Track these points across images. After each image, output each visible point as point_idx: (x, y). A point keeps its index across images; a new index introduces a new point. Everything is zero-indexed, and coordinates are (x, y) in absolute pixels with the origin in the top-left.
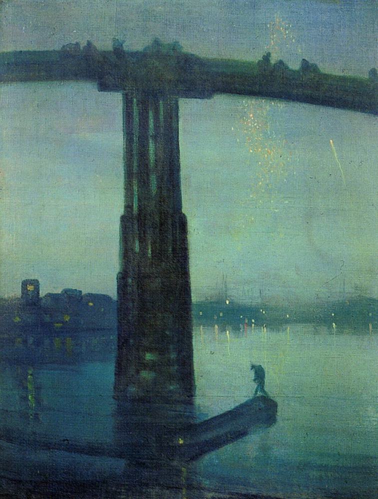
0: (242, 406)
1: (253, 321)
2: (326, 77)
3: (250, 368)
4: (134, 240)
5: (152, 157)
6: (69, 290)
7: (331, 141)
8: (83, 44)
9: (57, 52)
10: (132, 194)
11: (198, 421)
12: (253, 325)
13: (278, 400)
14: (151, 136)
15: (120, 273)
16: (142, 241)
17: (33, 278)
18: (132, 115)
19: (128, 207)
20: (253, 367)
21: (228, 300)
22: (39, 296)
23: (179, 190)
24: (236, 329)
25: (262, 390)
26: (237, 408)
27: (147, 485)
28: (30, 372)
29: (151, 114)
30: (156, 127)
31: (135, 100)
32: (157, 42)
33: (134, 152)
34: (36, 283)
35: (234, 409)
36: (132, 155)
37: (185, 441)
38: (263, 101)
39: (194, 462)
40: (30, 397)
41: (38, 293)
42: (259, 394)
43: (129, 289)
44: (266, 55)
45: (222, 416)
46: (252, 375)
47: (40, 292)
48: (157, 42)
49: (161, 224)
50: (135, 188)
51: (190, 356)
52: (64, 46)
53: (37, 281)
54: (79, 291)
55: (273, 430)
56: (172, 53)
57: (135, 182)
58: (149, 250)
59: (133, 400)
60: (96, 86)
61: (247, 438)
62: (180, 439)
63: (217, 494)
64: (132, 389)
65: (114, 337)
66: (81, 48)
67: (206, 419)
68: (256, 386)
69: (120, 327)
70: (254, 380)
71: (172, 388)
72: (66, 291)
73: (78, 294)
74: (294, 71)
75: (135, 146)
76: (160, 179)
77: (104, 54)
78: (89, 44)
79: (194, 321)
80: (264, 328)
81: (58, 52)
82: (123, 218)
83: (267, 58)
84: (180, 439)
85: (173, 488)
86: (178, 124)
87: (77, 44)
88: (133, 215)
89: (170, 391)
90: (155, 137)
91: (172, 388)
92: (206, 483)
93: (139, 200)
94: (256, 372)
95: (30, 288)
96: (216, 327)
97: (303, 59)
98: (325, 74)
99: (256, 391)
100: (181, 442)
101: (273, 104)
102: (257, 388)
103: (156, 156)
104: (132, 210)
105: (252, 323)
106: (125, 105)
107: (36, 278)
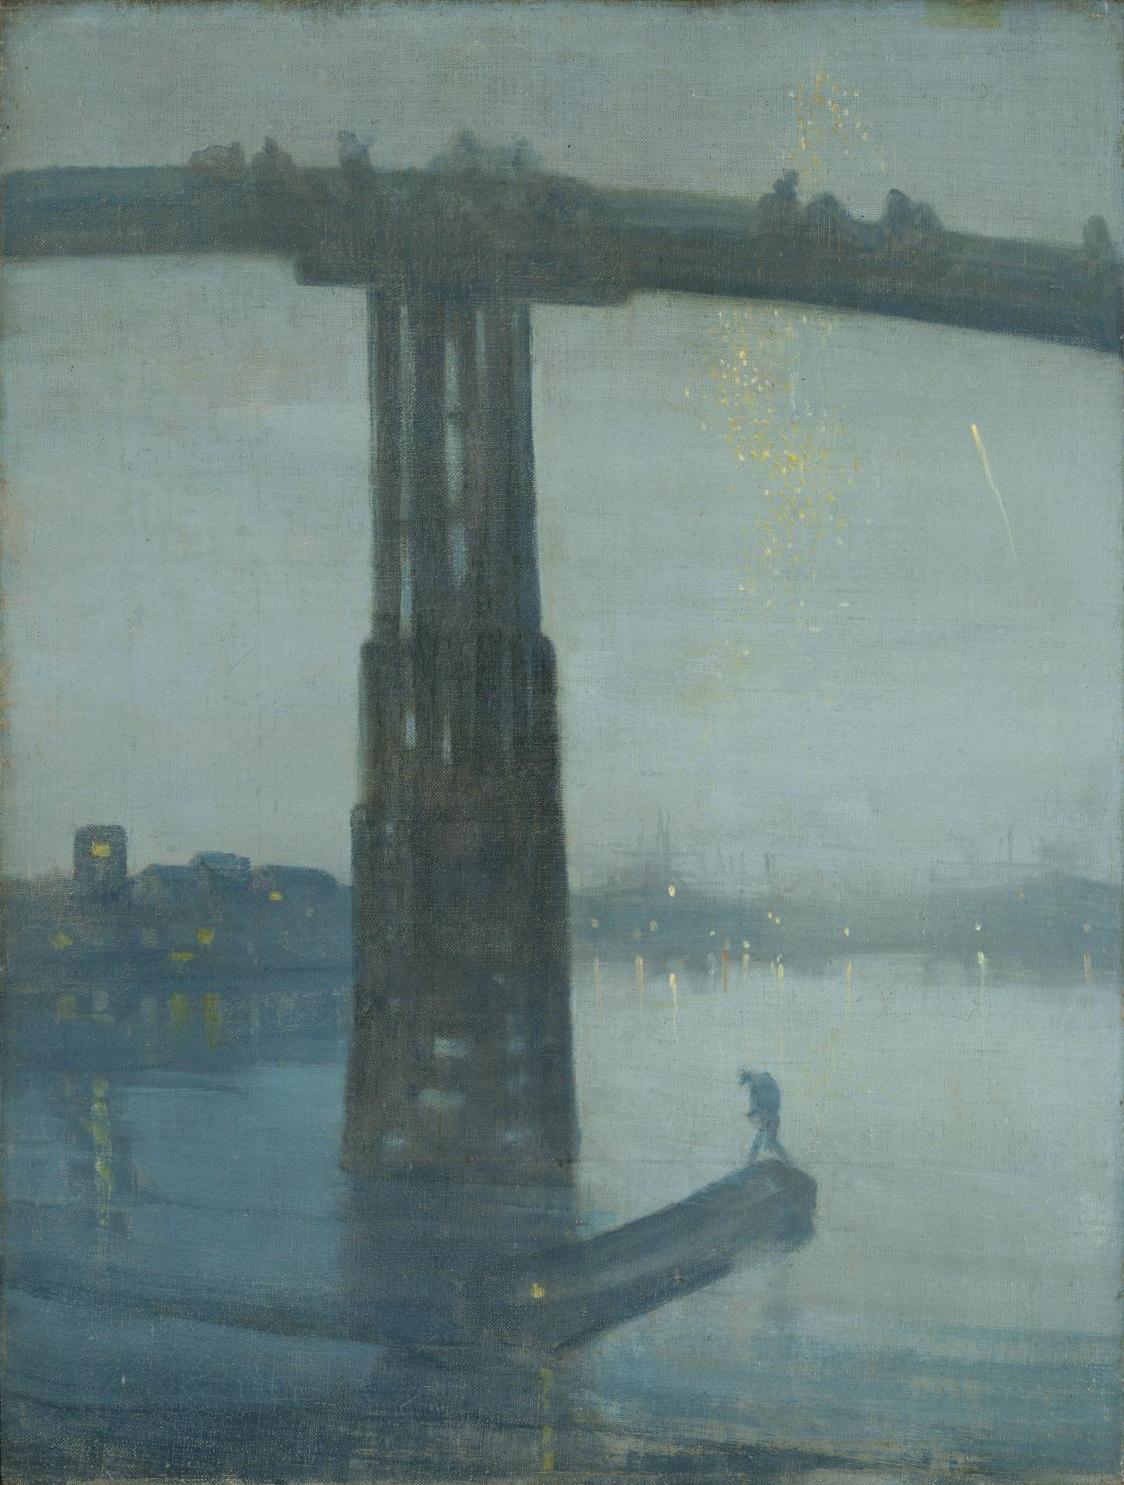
0: (715, 1190)
1: (747, 945)
2: (961, 240)
5: (454, 477)
6: (214, 857)
8: (252, 150)
9: (176, 169)
10: (398, 580)
11: (585, 1234)
12: (747, 957)
14: (452, 415)
15: (358, 808)
18: (397, 356)
19: (386, 618)
21: (673, 884)
22: (125, 873)
25: (773, 1142)
26: (697, 1198)
28: (99, 1092)
30: (468, 389)
31: (404, 311)
32: (467, 142)
34: (115, 837)
36: (396, 469)
38: (776, 312)
40: (98, 1163)
41: (124, 865)
42: (765, 1154)
46: (743, 1100)
47: (129, 862)
48: (467, 142)
49: (482, 670)
50: (406, 565)
52: (196, 154)
55: (805, 1257)
57: (405, 546)
60: (290, 271)
65: (344, 992)
66: (248, 160)
70: (750, 1115)
71: (510, 1137)
72: (204, 861)
74: (866, 227)
75: (405, 439)
76: (479, 541)
78: (271, 148)
79: (576, 946)
82: (372, 653)
83: (785, 189)
84: (535, 1285)
90: (463, 420)
91: (510, 1137)
95: (101, 850)
96: (640, 961)
97: (893, 191)
98: (955, 235)
99: (756, 1147)
100: (538, 1293)
102: (759, 1138)
103: (465, 472)
104: (397, 628)
107: (119, 822)
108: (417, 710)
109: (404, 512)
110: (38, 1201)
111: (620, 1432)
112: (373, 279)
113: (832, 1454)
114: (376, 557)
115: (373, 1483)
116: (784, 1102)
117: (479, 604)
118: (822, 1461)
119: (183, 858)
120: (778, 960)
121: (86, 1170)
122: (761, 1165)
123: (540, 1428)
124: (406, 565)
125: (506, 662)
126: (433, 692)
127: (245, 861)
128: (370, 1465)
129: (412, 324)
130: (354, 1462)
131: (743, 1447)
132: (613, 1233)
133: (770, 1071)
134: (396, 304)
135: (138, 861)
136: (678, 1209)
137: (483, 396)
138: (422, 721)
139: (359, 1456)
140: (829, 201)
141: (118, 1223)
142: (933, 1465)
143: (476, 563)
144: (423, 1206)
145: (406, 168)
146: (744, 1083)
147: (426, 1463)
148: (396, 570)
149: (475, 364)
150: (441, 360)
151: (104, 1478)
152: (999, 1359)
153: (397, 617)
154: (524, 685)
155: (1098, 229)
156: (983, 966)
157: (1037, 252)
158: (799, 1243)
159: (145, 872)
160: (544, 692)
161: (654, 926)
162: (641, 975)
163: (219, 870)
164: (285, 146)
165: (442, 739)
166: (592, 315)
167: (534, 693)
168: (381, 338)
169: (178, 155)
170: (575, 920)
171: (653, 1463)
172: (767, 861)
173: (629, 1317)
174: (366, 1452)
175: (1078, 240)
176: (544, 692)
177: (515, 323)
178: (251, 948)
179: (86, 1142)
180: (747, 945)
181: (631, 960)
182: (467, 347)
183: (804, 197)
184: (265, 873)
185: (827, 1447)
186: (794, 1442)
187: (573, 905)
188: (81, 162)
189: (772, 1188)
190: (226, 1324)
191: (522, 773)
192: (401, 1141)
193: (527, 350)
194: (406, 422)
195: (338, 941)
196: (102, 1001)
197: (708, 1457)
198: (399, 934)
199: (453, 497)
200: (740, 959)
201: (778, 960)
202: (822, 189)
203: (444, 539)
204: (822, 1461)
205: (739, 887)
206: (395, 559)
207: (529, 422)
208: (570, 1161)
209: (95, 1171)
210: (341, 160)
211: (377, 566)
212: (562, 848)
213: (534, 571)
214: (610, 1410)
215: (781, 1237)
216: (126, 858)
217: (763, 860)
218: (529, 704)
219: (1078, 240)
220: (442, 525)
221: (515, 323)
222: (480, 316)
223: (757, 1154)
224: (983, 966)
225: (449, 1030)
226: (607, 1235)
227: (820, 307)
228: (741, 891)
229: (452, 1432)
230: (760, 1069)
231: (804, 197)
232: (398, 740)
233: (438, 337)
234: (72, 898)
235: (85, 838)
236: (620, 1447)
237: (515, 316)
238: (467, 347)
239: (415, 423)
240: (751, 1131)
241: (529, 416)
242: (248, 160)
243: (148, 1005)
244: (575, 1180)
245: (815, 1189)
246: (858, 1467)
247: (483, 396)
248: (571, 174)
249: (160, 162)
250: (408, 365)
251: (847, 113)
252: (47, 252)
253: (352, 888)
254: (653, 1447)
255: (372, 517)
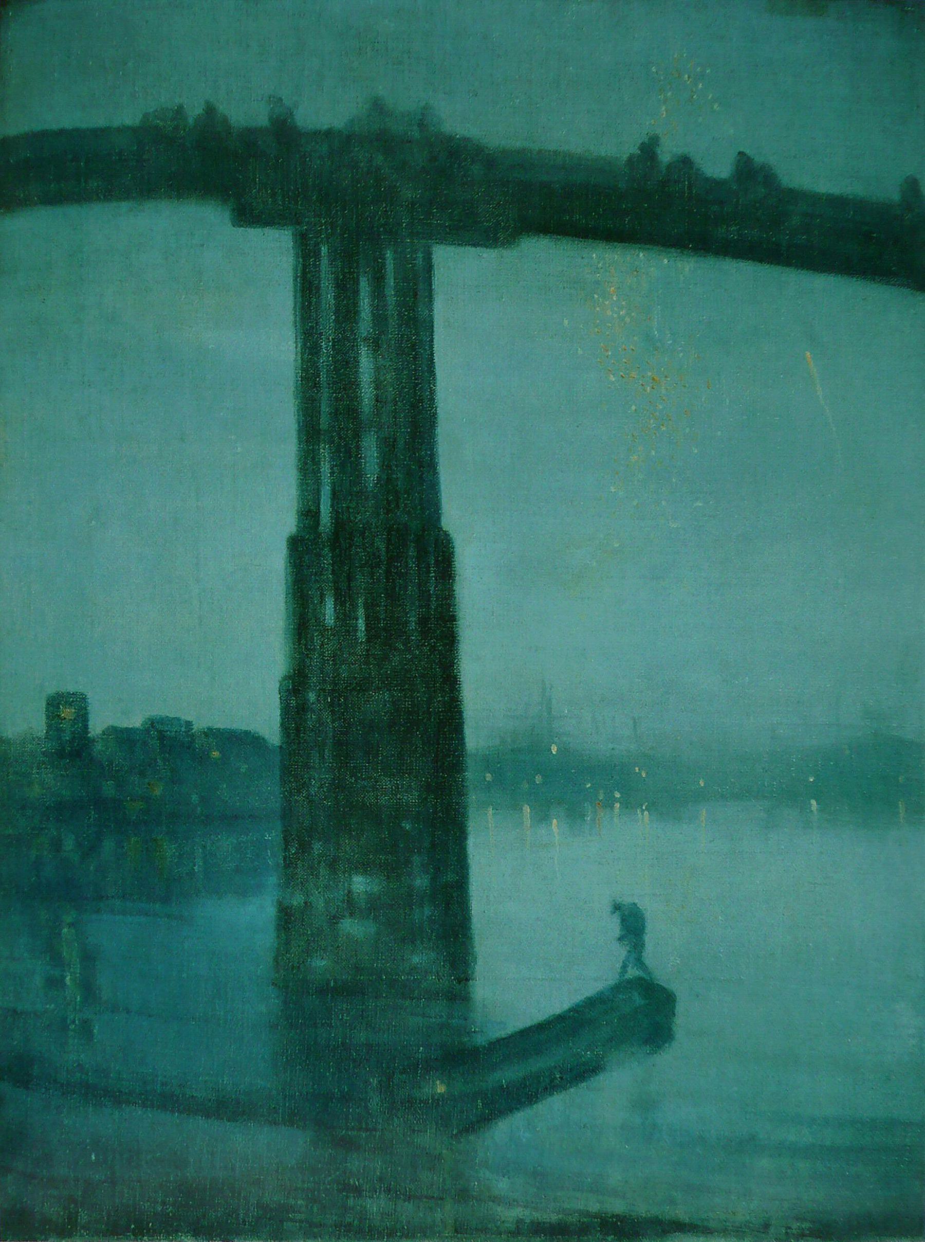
0: (591, 1003)
1: (618, 795)
2: (795, 195)
3: (609, 909)
4: (322, 596)
5: (367, 393)
6: (163, 721)
7: (329, 700)
8: (194, 111)
9: (129, 128)
10: (318, 482)
11: (480, 1040)
12: (617, 805)
13: (674, 986)
14: (365, 339)
15: (286, 678)
16: (343, 598)
17: (71, 688)
18: (318, 288)
19: (309, 515)
20: (617, 907)
21: (555, 743)
22: (88, 733)
23: (434, 486)
24: (575, 815)
25: (639, 962)
26: (575, 1009)
27: (358, 1191)
28: (68, 919)
29: (364, 286)
30: (379, 319)
31: (324, 250)
32: (378, 106)
33: (323, 377)
34: (79, 702)
35: (570, 1010)
36: (316, 385)
37: (448, 1085)
38: (641, 255)
39: (472, 1137)
40: (68, 978)
41: (86, 727)
42: (633, 972)
43: (311, 719)
44: (646, 140)
45: (541, 1027)
46: (614, 926)
47: (91, 724)
48: (378, 106)
49: (391, 560)
50: (325, 468)
51: (461, 885)
52: (146, 115)
53: (84, 699)
54: (186, 722)
55: (666, 1058)
56: (416, 135)
57: (325, 452)
58: (360, 621)
59: (323, 991)
60: (227, 215)
61: (601, 1080)
62: (438, 1082)
63: (527, 1212)
64: (320, 963)
65: (273, 835)
66: (191, 121)
67: (502, 1034)
68: (624, 953)
69: (287, 813)
70: (620, 939)
71: (416, 959)
72: (153, 723)
73: (183, 729)
74: (719, 184)
75: (324, 359)
76: (388, 446)
77: (250, 136)
78: (210, 110)
79: (473, 798)
80: (643, 811)
81: (133, 130)
82: (295, 543)
83: (649, 150)
84: (438, 1082)
85: (420, 1198)
86: (431, 310)
87: (179, 111)
88: (319, 535)
89: (413, 969)
90: (375, 345)
91: (416, 959)
92: (502, 1185)
93: (334, 495)
94: (623, 920)
95: (68, 713)
96: (527, 809)
97: (740, 153)
98: (791, 191)
99: (624, 967)
100: (441, 1089)
101: (666, 261)
102: (627, 958)
103: (377, 388)
104: (318, 523)
105: (616, 800)
106: (301, 260)
107: (79, 688)
108: (335, 594)
109: (324, 422)
110: (20, 1008)
111: (511, 1203)
112: (299, 223)
113: (687, 1221)
114: (299, 460)
115: (304, 1241)
116: (649, 927)
117: (389, 503)
118: (679, 1227)
119: (136, 721)
120: (644, 808)
121: (55, 983)
122: (629, 982)
123: (442, 1199)
124: (325, 468)
125: (412, 552)
126: (350, 578)
127: (189, 724)
128: (301, 1227)
129: (332, 261)
130: (287, 1225)
131: (613, 1216)
132: (504, 1039)
133: (636, 901)
134: (317, 244)
135: (97, 726)
136: (560, 1018)
137: (393, 322)
138: (340, 600)
139: (292, 1220)
140: (686, 161)
141: (86, 1029)
142: (772, 1230)
143: (386, 466)
144: (342, 1016)
145: (325, 127)
146: (614, 913)
147: (348, 1228)
148: (317, 472)
149: (384, 296)
150: (356, 292)
151: (80, 1236)
152: (828, 1143)
153: (318, 512)
154: (429, 572)
155: (912, 184)
156: (815, 812)
157: (860, 205)
158: (659, 1047)
159: (104, 733)
160: (443, 578)
161: (538, 779)
162: (528, 822)
163: (167, 731)
164: (222, 108)
165: (357, 619)
166: (485, 255)
167: (436, 579)
168: (304, 273)
169: (129, 117)
170: (471, 775)
171: (538, 1228)
172: (635, 722)
173: (517, 1109)
174: (299, 1216)
175: (896, 197)
176: (443, 578)
177: (420, 262)
178: (195, 798)
179: (57, 959)
180: (618, 795)
181: (517, 808)
182: (378, 280)
183: (666, 155)
184: (206, 735)
185: (682, 1213)
186: (655, 1211)
187: (470, 762)
188: (55, 127)
189: (638, 1000)
190: (179, 1111)
191: (426, 649)
192: (324, 963)
193: (430, 285)
194: (325, 346)
195: (278, 759)
196: (69, 844)
197: (583, 1223)
198: (321, 787)
199: (366, 410)
200: (612, 807)
201: (644, 808)
202: (680, 151)
203: (358, 447)
204: (679, 1227)
205: (611, 746)
206: (316, 462)
207: (431, 347)
208: (467, 980)
209: (65, 984)
210: (271, 118)
211: (301, 468)
212: (460, 713)
213: (435, 473)
214: (501, 1185)
215: (646, 1042)
216: (88, 721)
217: (631, 722)
218: (432, 588)
219: (896, 197)
220: (357, 436)
221: (420, 262)
222: (389, 254)
223: (626, 972)
224: (815, 812)
225: (364, 867)
226: (499, 1041)
227: (678, 251)
228: (613, 749)
229: (369, 1201)
230: (628, 900)
231: (666, 155)
232: (319, 622)
233: (354, 272)
234: (44, 753)
235: (55, 703)
236: (511, 1215)
237: (420, 255)
238: (378, 280)
239: (333, 346)
240: (621, 952)
241: (432, 341)
242: (191, 121)
243: (108, 845)
244: (472, 996)
245: (674, 1001)
246: (707, 1231)
247: (393, 322)
248: (467, 134)
249: (116, 123)
250: (328, 296)
251: (700, 86)
252: (24, 203)
253: (281, 747)
254: (537, 1216)
255: (297, 426)
